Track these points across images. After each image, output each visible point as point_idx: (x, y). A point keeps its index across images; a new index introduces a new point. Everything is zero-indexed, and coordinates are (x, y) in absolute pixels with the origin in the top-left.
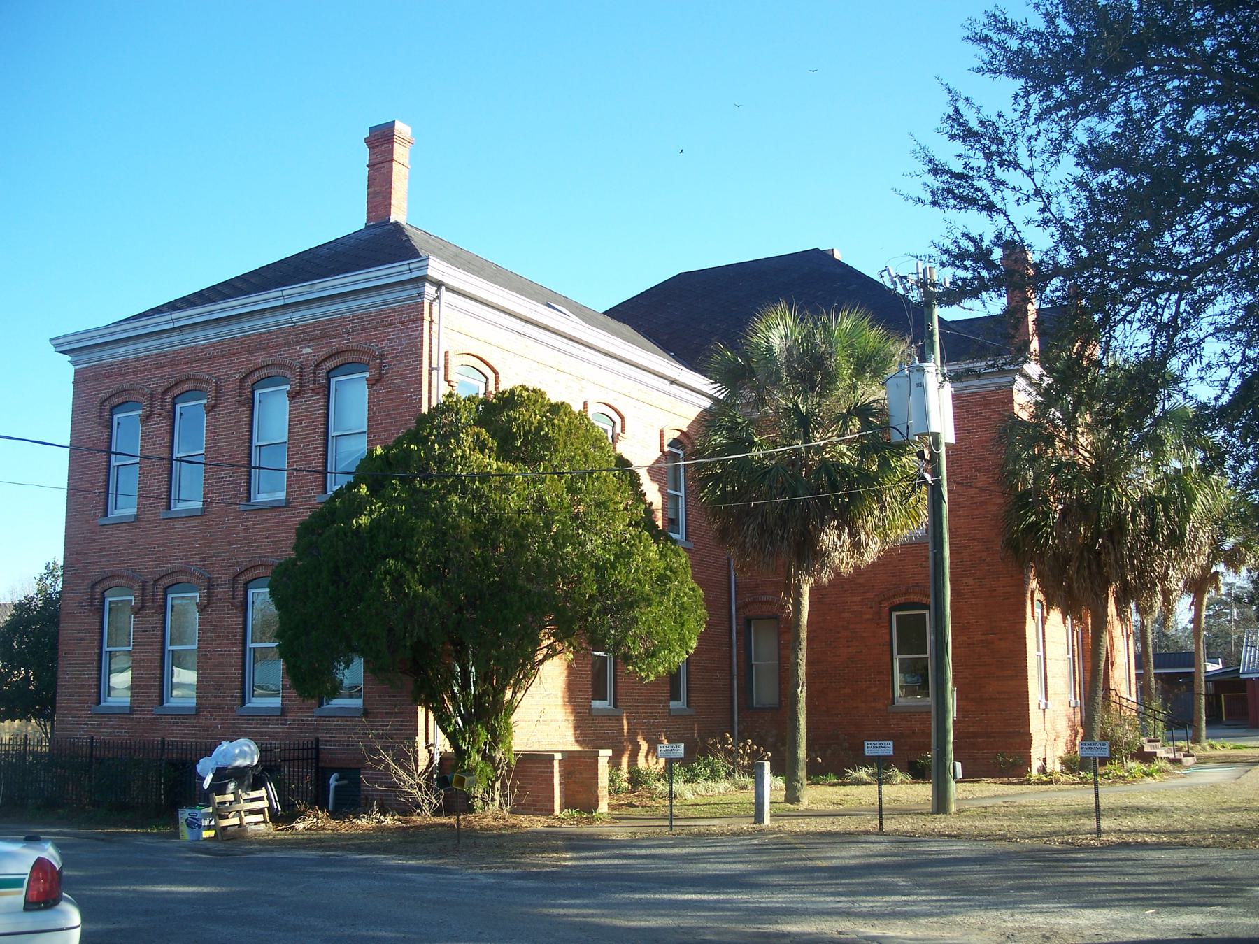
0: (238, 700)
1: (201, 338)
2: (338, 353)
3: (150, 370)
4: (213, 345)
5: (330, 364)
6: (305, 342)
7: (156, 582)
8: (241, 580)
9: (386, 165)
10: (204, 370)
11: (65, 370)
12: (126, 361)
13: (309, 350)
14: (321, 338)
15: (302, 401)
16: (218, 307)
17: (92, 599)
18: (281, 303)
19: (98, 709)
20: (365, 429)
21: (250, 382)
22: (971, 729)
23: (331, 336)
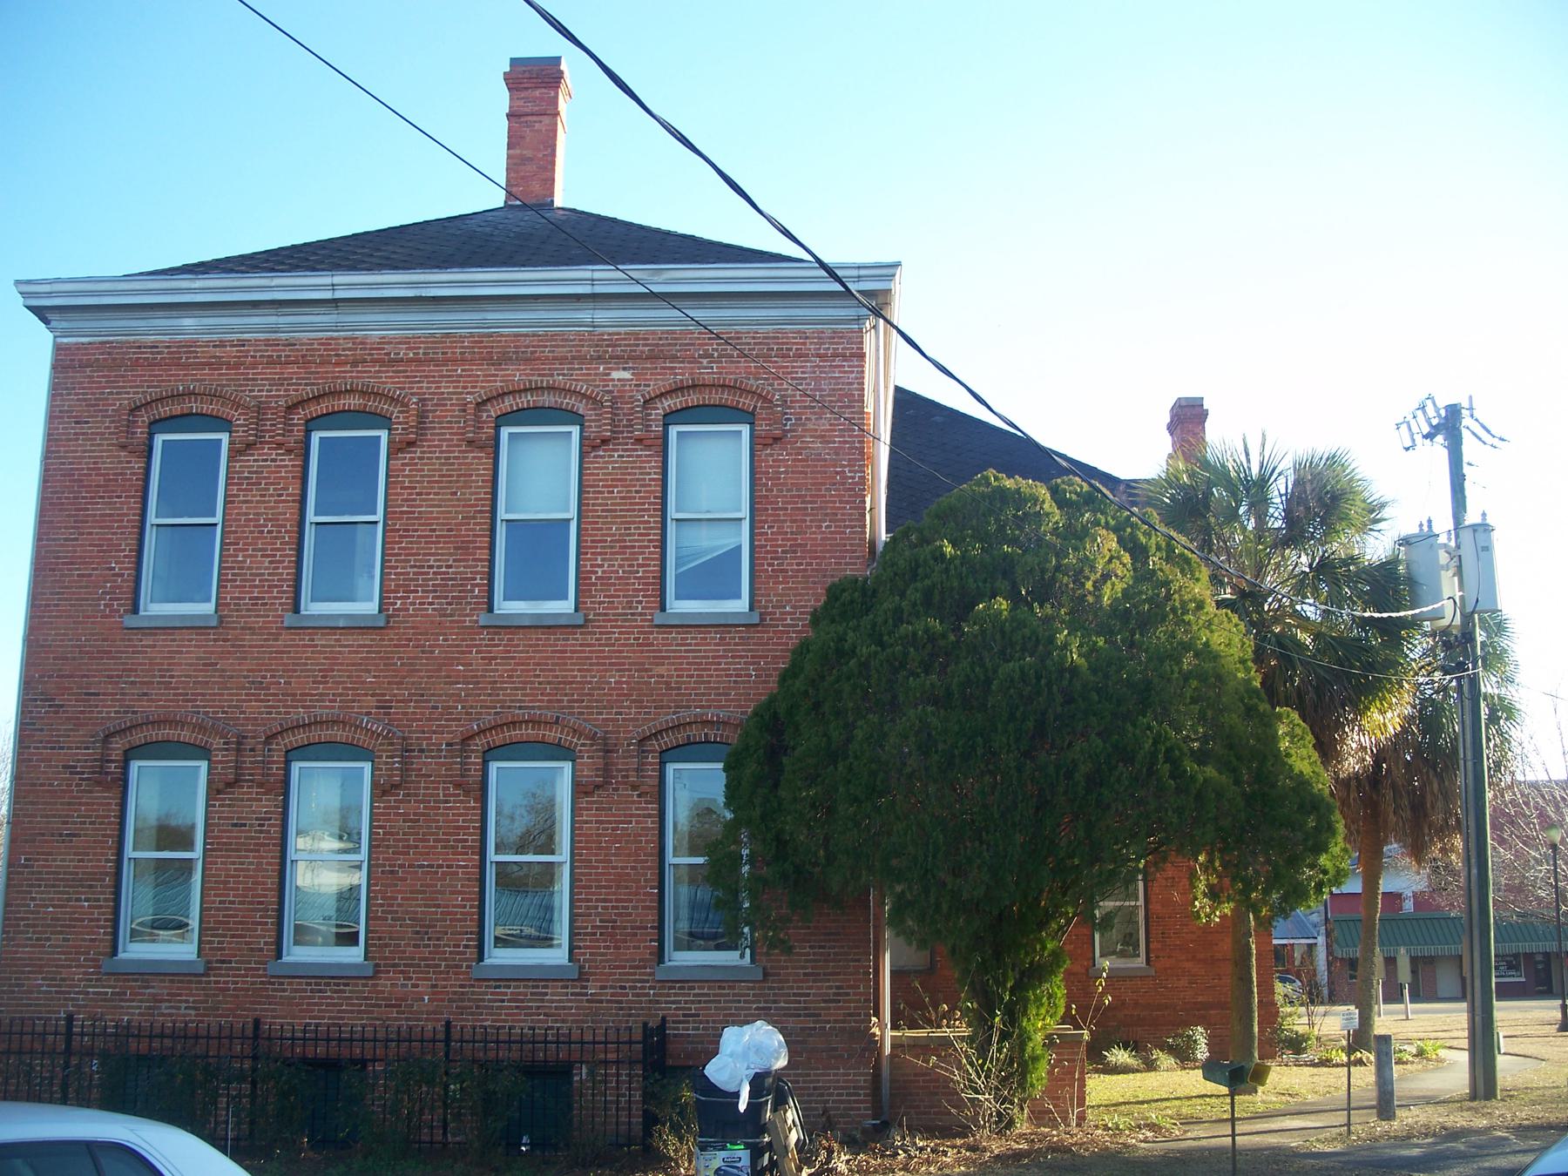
0: (471, 953)
1: (377, 327)
2: (694, 386)
3: (254, 365)
4: (405, 341)
5: (669, 403)
6: (620, 360)
7: (270, 738)
8: (479, 743)
9: (546, 120)
10: (388, 381)
11: (39, 343)
12: (192, 344)
13: (627, 375)
14: (652, 357)
15: (613, 459)
16: (198, 284)
17: (105, 760)
18: (586, 290)
19: (107, 965)
20: (745, 512)
21: (493, 411)
22: (1200, 999)
23: (674, 358)
